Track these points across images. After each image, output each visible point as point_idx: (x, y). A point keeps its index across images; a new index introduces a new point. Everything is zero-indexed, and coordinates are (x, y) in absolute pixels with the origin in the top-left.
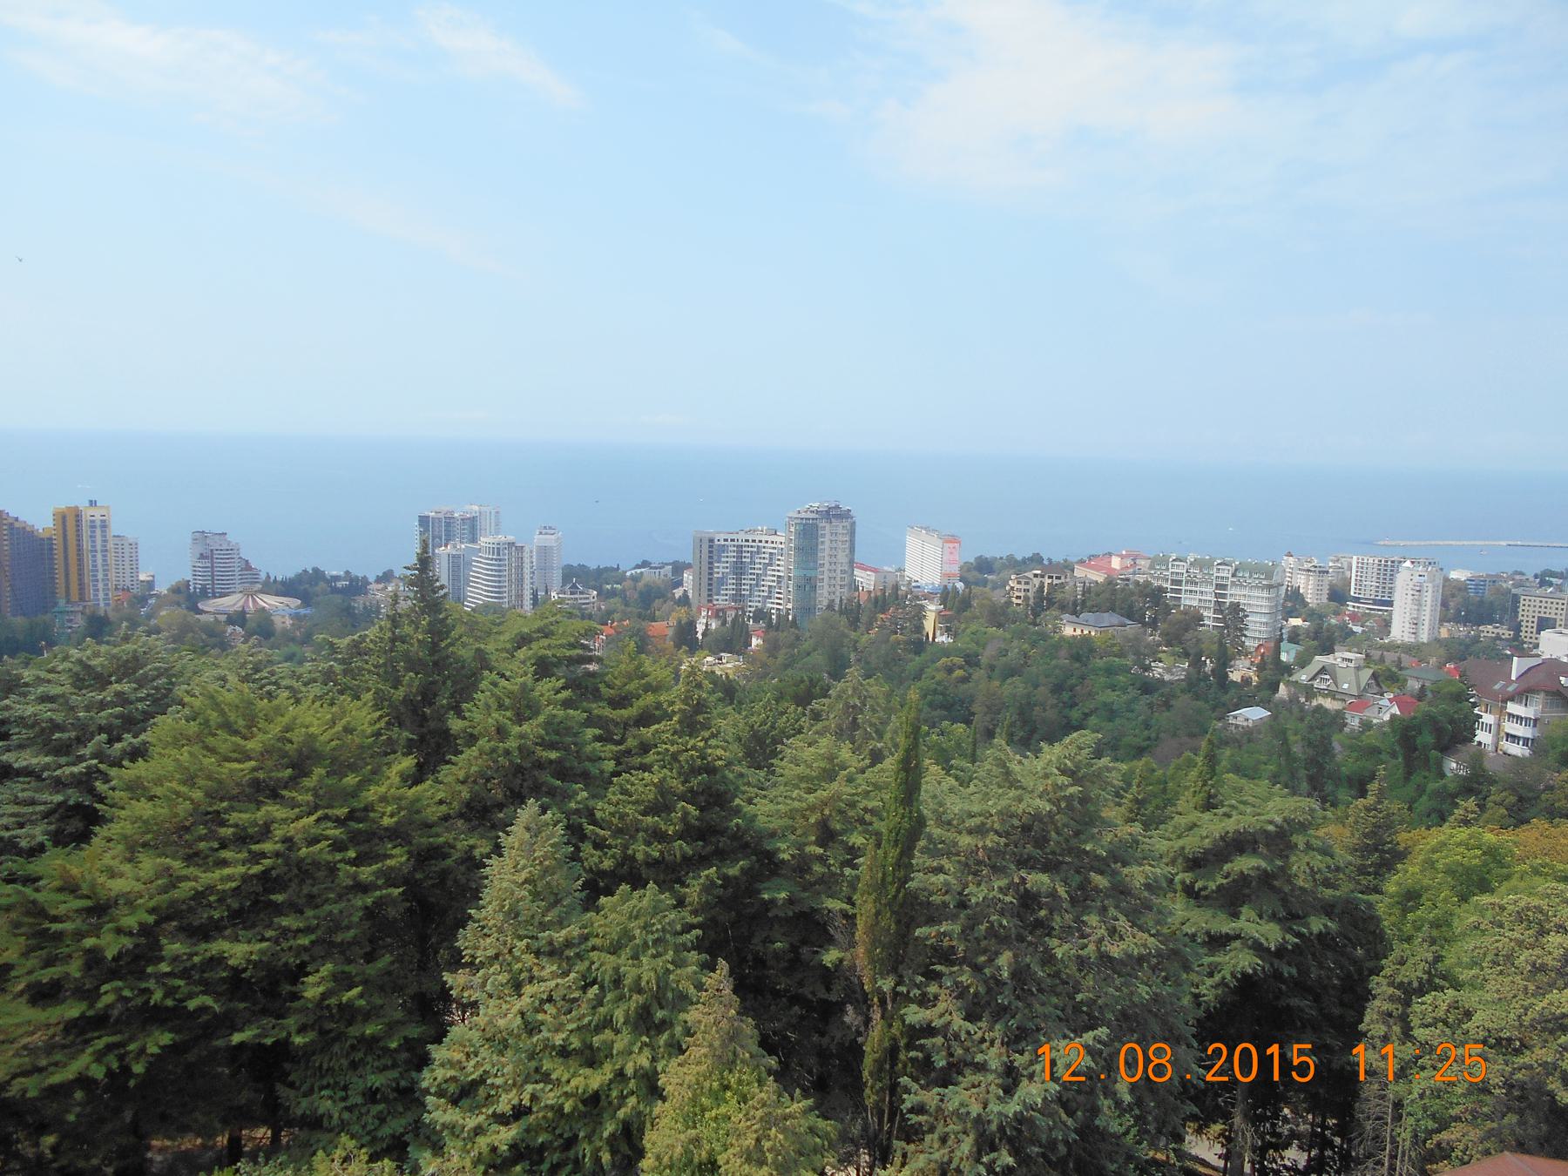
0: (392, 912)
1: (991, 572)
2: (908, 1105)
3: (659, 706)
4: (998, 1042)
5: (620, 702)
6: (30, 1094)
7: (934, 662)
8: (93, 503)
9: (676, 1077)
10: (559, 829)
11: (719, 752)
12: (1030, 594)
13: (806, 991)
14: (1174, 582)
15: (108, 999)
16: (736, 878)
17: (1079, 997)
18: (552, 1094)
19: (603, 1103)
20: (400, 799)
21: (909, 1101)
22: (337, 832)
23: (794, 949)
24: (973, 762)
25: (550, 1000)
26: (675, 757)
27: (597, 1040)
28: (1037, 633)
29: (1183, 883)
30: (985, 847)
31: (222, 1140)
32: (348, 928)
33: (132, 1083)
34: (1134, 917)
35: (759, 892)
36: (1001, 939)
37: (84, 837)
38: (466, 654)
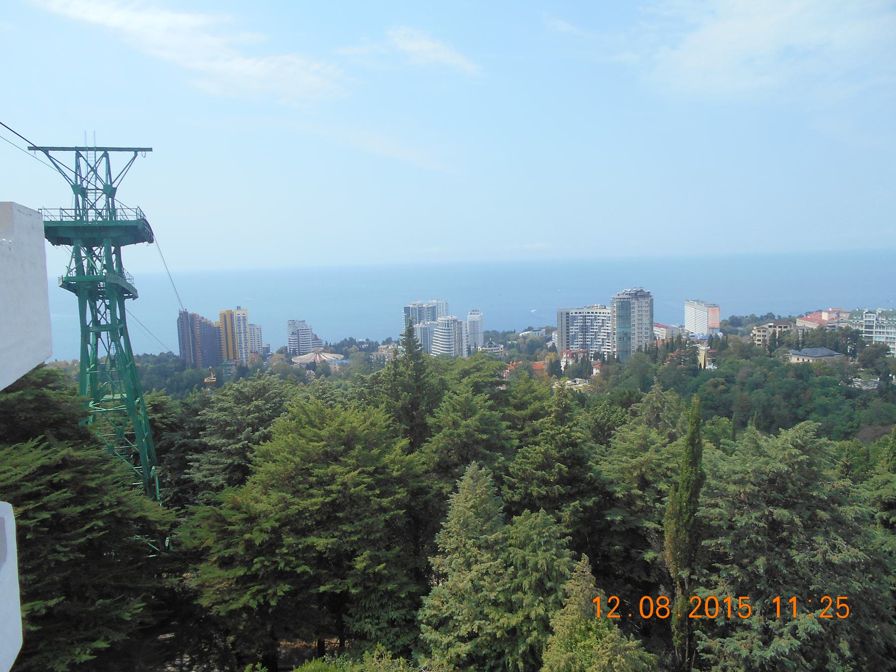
0: (399, 523)
1: (740, 325)
2: (701, 647)
3: (543, 408)
4: (758, 612)
5: (521, 406)
6: (222, 614)
7: (705, 381)
8: (239, 308)
9: (560, 621)
10: (489, 478)
11: (579, 434)
12: (767, 338)
13: (635, 576)
14: (867, 327)
15: (258, 566)
16: (591, 508)
17: (812, 588)
18: (489, 627)
19: (518, 633)
20: (402, 461)
21: (701, 645)
22: (369, 480)
23: (627, 550)
24: (735, 440)
25: (487, 573)
26: (553, 437)
27: (514, 597)
28: (773, 362)
29: (881, 518)
30: (745, 492)
31: (315, 644)
32: (377, 531)
33: (270, 610)
34: (848, 539)
35: (604, 516)
36: (760, 550)
37: (242, 482)
38: (434, 381)
